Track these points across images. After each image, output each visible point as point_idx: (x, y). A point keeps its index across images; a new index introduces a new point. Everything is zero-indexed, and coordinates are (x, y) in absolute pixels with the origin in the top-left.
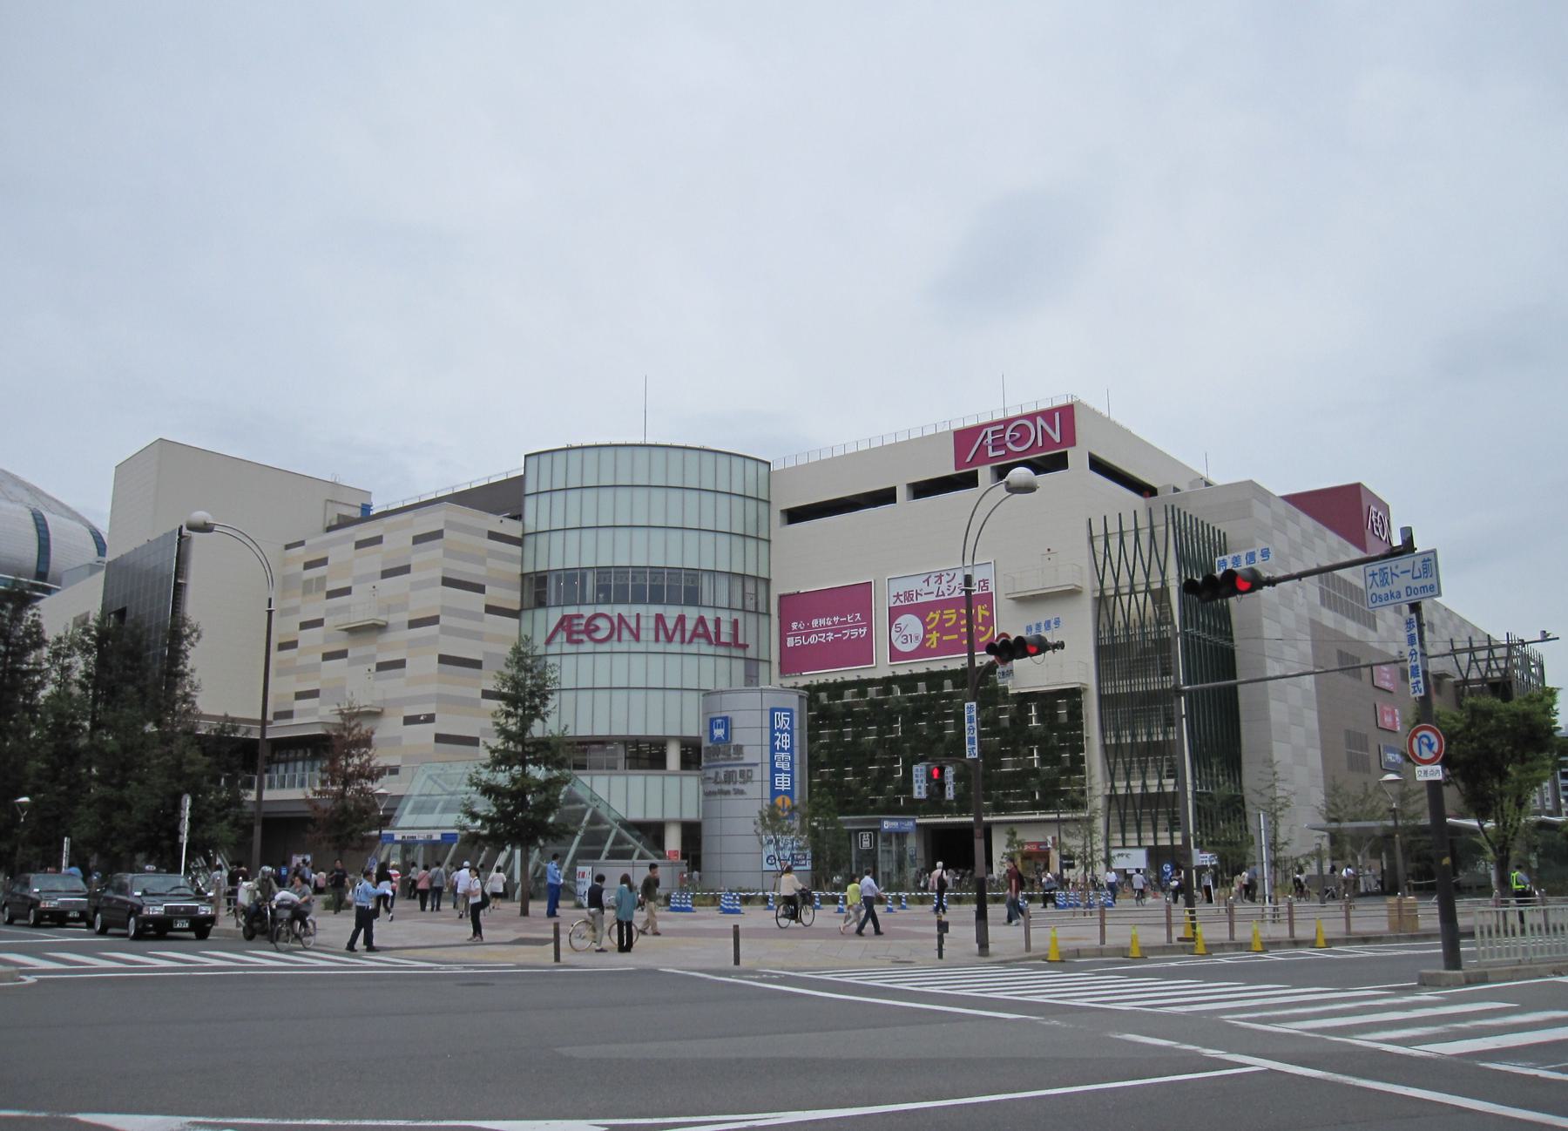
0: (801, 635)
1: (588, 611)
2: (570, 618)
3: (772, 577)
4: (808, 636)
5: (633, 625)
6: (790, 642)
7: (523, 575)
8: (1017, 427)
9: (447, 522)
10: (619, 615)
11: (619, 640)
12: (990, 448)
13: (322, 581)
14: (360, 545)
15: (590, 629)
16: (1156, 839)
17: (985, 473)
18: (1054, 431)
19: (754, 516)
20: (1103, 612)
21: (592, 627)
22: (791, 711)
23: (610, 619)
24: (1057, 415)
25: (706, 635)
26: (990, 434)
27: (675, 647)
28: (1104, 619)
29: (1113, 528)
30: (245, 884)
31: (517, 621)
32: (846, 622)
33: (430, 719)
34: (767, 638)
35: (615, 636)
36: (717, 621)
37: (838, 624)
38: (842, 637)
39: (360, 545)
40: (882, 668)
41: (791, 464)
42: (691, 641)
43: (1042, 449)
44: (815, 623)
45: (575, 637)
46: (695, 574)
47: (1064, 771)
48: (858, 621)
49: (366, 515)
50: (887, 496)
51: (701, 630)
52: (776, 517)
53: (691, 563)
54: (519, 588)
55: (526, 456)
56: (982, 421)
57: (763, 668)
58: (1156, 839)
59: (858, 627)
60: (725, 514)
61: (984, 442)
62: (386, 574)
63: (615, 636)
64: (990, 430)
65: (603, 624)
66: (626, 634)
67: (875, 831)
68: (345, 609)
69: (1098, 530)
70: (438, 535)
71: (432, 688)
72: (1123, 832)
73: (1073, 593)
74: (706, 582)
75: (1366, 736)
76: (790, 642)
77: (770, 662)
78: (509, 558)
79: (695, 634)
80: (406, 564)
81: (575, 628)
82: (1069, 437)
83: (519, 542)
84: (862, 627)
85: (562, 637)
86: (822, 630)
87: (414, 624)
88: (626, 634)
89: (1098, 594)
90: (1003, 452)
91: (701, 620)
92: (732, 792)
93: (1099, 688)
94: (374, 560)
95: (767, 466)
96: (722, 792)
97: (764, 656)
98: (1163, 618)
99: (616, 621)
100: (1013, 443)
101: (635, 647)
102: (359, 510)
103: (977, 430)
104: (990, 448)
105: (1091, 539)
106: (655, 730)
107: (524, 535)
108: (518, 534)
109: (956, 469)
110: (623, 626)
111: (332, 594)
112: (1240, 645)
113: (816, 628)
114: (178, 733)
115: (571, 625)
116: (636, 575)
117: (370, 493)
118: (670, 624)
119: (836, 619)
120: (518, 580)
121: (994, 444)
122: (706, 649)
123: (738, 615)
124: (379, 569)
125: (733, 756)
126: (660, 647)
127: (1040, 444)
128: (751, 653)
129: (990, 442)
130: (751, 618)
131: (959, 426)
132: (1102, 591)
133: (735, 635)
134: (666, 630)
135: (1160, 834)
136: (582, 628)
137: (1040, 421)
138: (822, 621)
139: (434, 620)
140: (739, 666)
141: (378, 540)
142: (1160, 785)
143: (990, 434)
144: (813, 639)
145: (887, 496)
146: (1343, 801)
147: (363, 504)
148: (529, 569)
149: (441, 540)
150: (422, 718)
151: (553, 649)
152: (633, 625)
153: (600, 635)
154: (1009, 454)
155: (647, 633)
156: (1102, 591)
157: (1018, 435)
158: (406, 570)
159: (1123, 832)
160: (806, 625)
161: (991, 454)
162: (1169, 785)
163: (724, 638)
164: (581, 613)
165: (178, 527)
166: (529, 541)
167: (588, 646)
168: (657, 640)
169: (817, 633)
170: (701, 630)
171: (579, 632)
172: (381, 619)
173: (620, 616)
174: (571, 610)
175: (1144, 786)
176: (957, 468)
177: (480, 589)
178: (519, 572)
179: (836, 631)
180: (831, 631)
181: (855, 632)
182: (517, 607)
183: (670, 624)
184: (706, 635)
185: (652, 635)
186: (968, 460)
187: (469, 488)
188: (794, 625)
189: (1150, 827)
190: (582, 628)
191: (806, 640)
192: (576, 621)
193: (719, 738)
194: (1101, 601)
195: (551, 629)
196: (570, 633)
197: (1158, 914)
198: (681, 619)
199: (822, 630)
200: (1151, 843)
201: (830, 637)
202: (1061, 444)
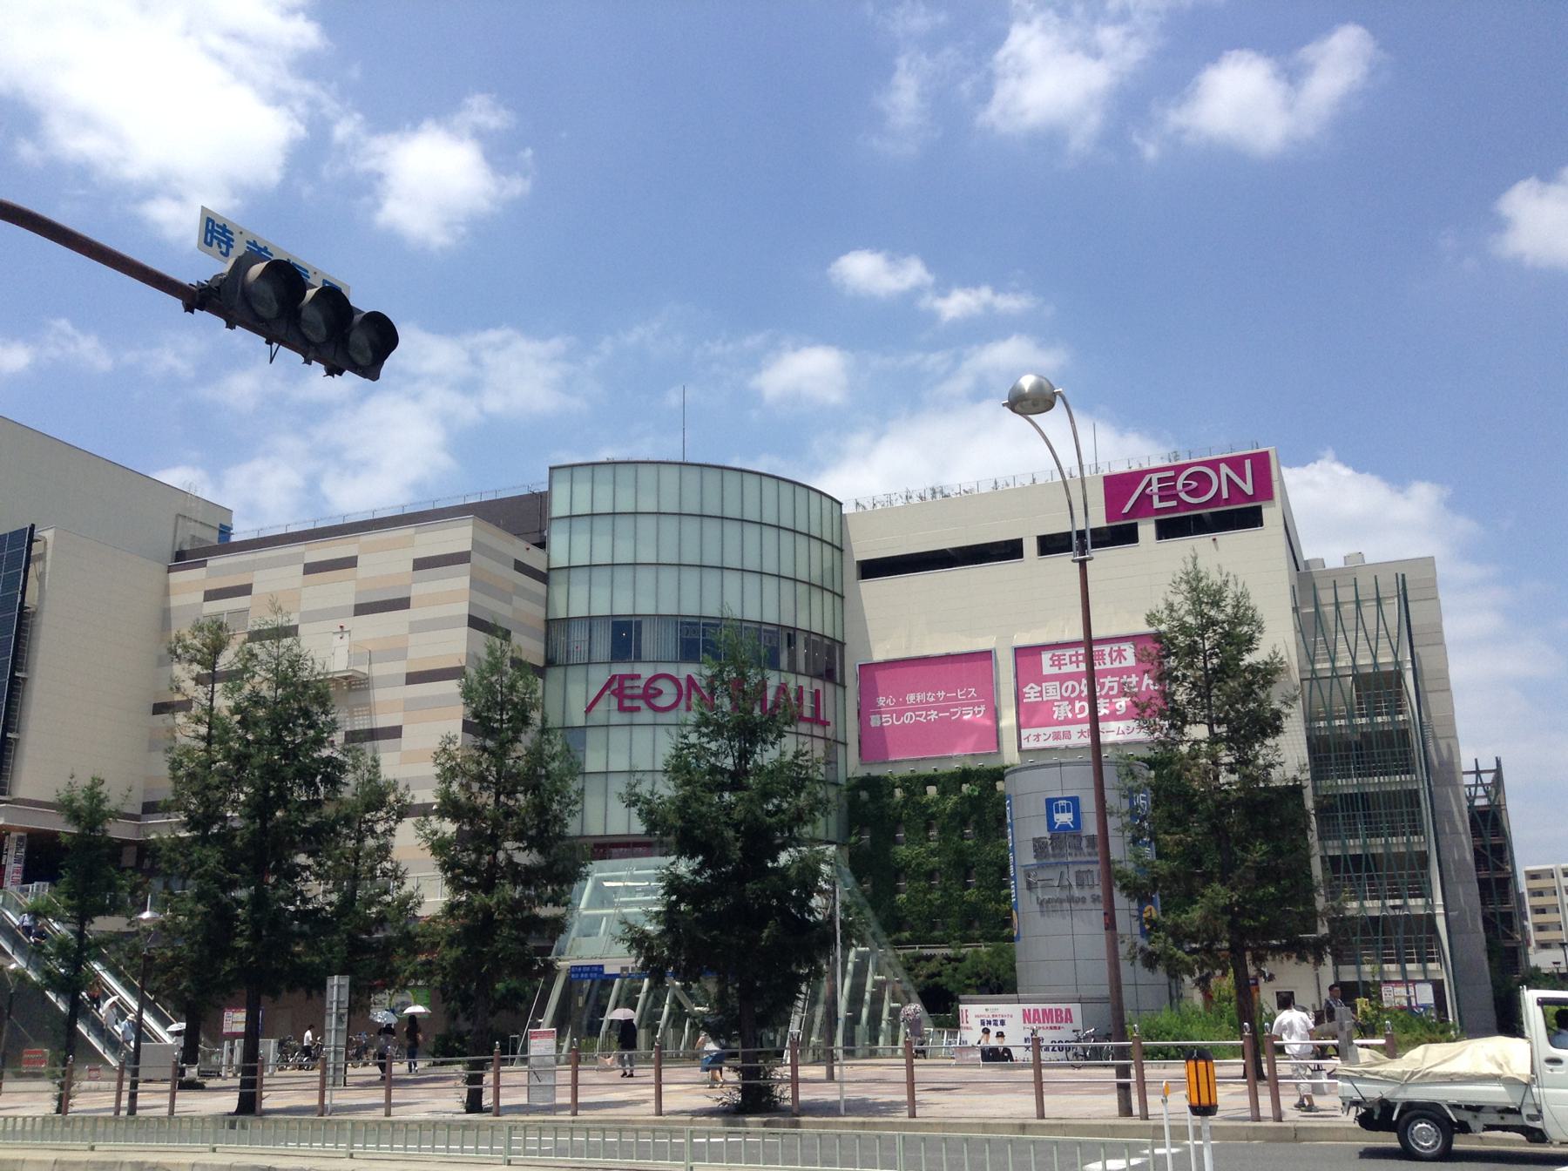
1: (646, 671)
2: (623, 677)
4: (900, 714)
9: (475, 542)
10: (689, 678)
12: (1156, 499)
14: (311, 569)
15: (650, 694)
17: (1147, 529)
18: (1245, 481)
19: (830, 565)
21: (651, 691)
22: (1075, 801)
24: (1248, 463)
26: (1155, 482)
29: (1346, 595)
32: (956, 698)
35: (683, 704)
36: (800, 689)
37: (944, 701)
38: (950, 717)
39: (311, 569)
43: (1227, 502)
44: (911, 698)
45: (627, 703)
48: (972, 698)
49: (225, 544)
50: (1010, 550)
52: (852, 571)
54: (543, 638)
55: (551, 468)
56: (1146, 467)
60: (809, 561)
61: (1148, 491)
62: (361, 609)
64: (1155, 477)
65: (667, 688)
77: (845, 744)
80: (407, 596)
81: (628, 692)
83: (543, 577)
85: (610, 703)
87: (414, 678)
90: (1174, 503)
92: (1089, 900)
93: (1315, 788)
94: (341, 590)
95: (838, 506)
96: (1071, 900)
100: (1186, 492)
102: (216, 534)
103: (1135, 477)
104: (1156, 499)
107: (549, 569)
108: (542, 568)
109: (1107, 522)
113: (912, 704)
115: (621, 687)
116: (707, 628)
119: (941, 694)
120: (542, 628)
121: (1161, 494)
123: (818, 684)
124: (351, 601)
125: (1085, 850)
127: (1225, 495)
129: (1156, 490)
130: (829, 687)
133: (816, 709)
136: (640, 691)
137: (1224, 469)
141: (350, 562)
143: (1155, 482)
145: (1010, 550)
147: (221, 526)
149: (207, 589)
150: (434, 807)
157: (1195, 484)
158: (403, 604)
160: (898, 700)
161: (1157, 504)
164: (635, 673)
165: (28, 526)
167: (646, 715)
169: (914, 710)
171: (632, 697)
173: (689, 678)
174: (622, 669)
176: (1109, 519)
179: (939, 709)
182: (540, 663)
186: (1126, 510)
187: (478, 500)
190: (640, 691)
192: (627, 683)
193: (1064, 827)
195: (594, 693)
196: (620, 694)
197: (314, 1084)
201: (933, 715)
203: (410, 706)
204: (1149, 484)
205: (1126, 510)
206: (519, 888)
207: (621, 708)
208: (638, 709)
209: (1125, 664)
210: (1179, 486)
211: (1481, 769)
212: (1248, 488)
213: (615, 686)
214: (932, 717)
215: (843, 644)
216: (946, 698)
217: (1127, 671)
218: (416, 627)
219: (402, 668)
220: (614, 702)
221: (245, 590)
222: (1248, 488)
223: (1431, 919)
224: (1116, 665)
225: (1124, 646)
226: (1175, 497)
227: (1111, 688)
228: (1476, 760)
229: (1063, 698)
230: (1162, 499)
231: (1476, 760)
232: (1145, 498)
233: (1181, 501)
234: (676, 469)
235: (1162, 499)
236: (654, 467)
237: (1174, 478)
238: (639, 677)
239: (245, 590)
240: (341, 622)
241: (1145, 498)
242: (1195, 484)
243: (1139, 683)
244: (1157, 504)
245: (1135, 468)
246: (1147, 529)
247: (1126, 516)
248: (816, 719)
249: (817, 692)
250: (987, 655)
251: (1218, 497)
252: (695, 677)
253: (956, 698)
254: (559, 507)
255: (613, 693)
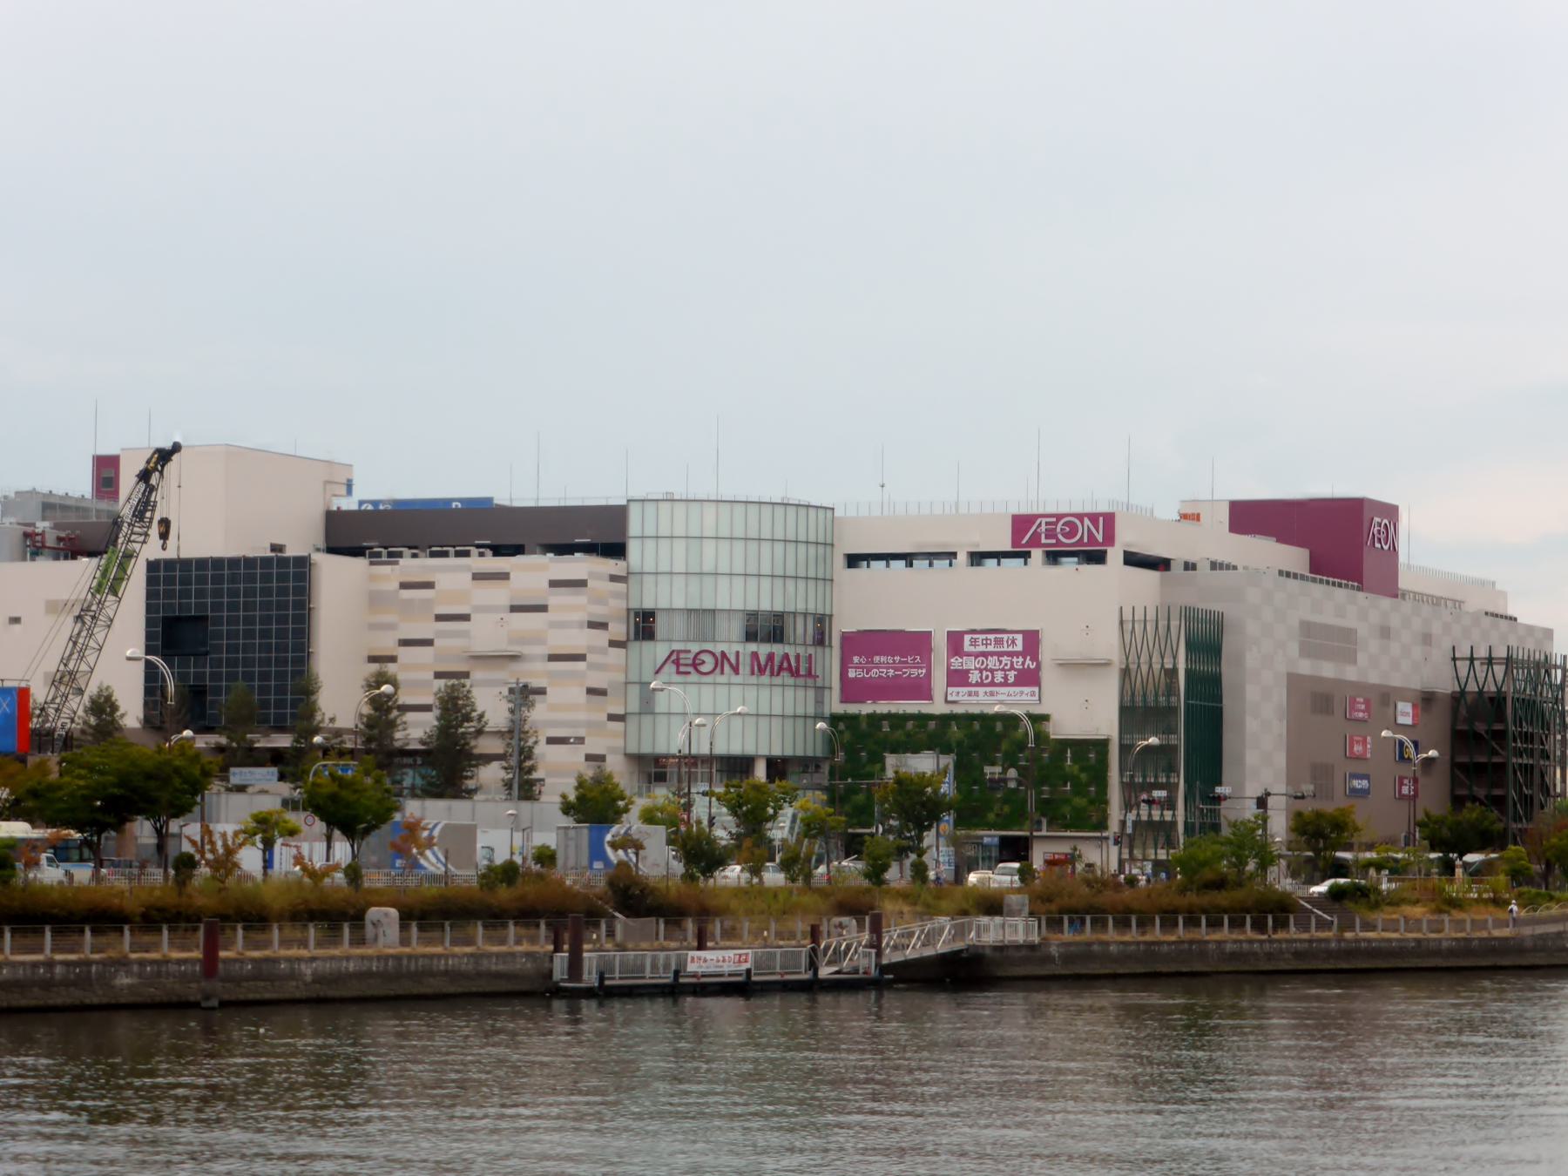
0: (863, 668)
2: (679, 652)
3: (834, 613)
5: (733, 661)
6: (852, 674)
7: (628, 610)
8: (1070, 522)
11: (722, 673)
12: (1043, 536)
13: (428, 603)
14: (477, 577)
15: (696, 664)
16: (1156, 854)
17: (1037, 554)
20: (1127, 680)
23: (713, 654)
24: (1101, 519)
25: (790, 668)
27: (765, 679)
28: (1127, 686)
30: (1513, 847)
31: (624, 650)
32: (906, 662)
33: (580, 740)
34: (830, 663)
35: (718, 670)
36: (798, 657)
39: (477, 577)
40: (937, 707)
41: (852, 513)
42: (778, 674)
44: (877, 659)
45: (682, 669)
46: (779, 616)
47: (1092, 802)
51: (785, 665)
52: (840, 562)
53: (779, 607)
54: (625, 620)
57: (827, 692)
58: (1156, 854)
59: (918, 668)
62: (515, 609)
63: (718, 670)
64: (1044, 520)
66: (727, 668)
67: (978, 844)
68: (465, 634)
69: (1127, 616)
70: (582, 583)
71: (582, 716)
72: (1144, 849)
73: (1107, 664)
74: (789, 621)
75: (1333, 766)
76: (852, 674)
77: (830, 688)
78: (616, 595)
79: (781, 668)
82: (1110, 538)
84: (922, 668)
86: (884, 667)
87: (553, 658)
88: (727, 668)
89: (1124, 666)
90: (1054, 541)
91: (786, 657)
93: (1121, 739)
94: (498, 594)
97: (827, 685)
98: (1171, 689)
99: (719, 658)
101: (736, 679)
104: (1043, 536)
105: (1122, 623)
106: (750, 750)
109: (1013, 546)
110: (725, 662)
111: (440, 618)
112: (1227, 703)
114: (846, 815)
115: (678, 659)
117: (351, 466)
118: (763, 660)
119: (897, 658)
122: (791, 681)
123: (811, 650)
126: (754, 679)
127: (1086, 540)
128: (819, 683)
129: (1044, 530)
131: (1015, 511)
132: (1127, 666)
134: (759, 665)
135: (1159, 851)
136: (690, 662)
137: (1087, 521)
138: (883, 659)
139: (580, 657)
140: (811, 693)
141: (504, 576)
142: (1162, 815)
144: (874, 673)
146: (705, 961)
148: (635, 605)
150: (572, 740)
151: (663, 676)
152: (733, 661)
153: (704, 669)
154: (1059, 543)
155: (745, 668)
156: (1127, 666)
158: (543, 608)
159: (1144, 849)
162: (1168, 815)
163: (802, 672)
166: (632, 579)
167: (694, 677)
168: (753, 673)
170: (785, 665)
172: (515, 649)
175: (1150, 815)
177: (603, 626)
178: (625, 607)
180: (892, 668)
181: (915, 672)
182: (623, 638)
183: (763, 660)
184: (790, 668)
185: (748, 669)
186: (1024, 542)
188: (856, 659)
189: (1153, 845)
191: (867, 673)
192: (682, 656)
194: (1125, 673)
195: (660, 662)
196: (677, 663)
198: (771, 657)
199: (884, 667)
200: (1153, 857)
202: (1102, 545)
203: (550, 675)
204: (1040, 525)
205: (1024, 542)
206: (46, 524)
207: (678, 673)
208: (689, 673)
209: (1016, 649)
210: (1058, 530)
211: (1475, 656)
212: (1100, 538)
213: (674, 657)
214: (890, 674)
215: (831, 616)
216: (900, 662)
217: (1017, 654)
218: (555, 625)
219: (545, 650)
220: (674, 668)
221: (429, 585)
222: (1100, 538)
223: (1173, 824)
224: (1010, 649)
225: (1016, 636)
226: (1054, 536)
227: (1006, 665)
228: (1454, 648)
229: (976, 669)
230: (1047, 537)
231: (1472, 648)
232: (1036, 535)
233: (1058, 539)
234: (714, 504)
235: (1047, 537)
236: (698, 504)
237: (1055, 524)
238: (689, 651)
239: (429, 585)
240: (502, 615)
241: (1036, 535)
242: (1068, 529)
243: (1023, 664)
244: (1044, 541)
245: (1029, 511)
246: (1037, 554)
247: (1024, 546)
248: (809, 674)
249: (810, 656)
250: (925, 637)
251: (1080, 541)
252: (726, 652)
253: (906, 662)
254: (634, 528)
255: (673, 662)
